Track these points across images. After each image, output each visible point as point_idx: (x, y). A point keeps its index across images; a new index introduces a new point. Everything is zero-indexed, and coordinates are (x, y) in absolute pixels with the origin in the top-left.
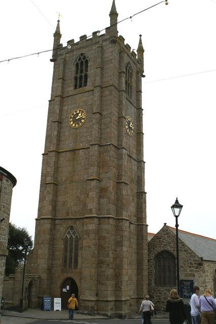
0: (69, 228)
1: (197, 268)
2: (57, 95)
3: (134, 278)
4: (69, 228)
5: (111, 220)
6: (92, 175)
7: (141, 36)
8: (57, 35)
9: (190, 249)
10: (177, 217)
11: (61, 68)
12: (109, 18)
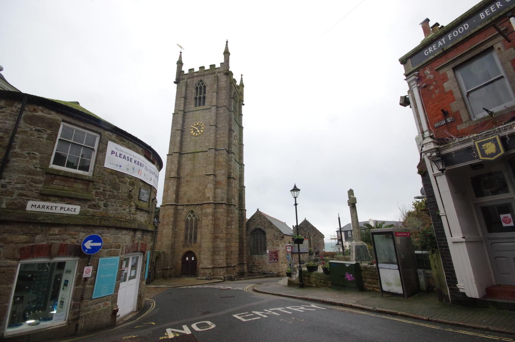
0: (190, 212)
1: (281, 240)
2: (181, 110)
4: (190, 212)
5: (224, 205)
6: (210, 171)
7: (242, 75)
8: (180, 63)
9: (276, 227)
10: (295, 198)
11: (184, 89)
12: (223, 56)
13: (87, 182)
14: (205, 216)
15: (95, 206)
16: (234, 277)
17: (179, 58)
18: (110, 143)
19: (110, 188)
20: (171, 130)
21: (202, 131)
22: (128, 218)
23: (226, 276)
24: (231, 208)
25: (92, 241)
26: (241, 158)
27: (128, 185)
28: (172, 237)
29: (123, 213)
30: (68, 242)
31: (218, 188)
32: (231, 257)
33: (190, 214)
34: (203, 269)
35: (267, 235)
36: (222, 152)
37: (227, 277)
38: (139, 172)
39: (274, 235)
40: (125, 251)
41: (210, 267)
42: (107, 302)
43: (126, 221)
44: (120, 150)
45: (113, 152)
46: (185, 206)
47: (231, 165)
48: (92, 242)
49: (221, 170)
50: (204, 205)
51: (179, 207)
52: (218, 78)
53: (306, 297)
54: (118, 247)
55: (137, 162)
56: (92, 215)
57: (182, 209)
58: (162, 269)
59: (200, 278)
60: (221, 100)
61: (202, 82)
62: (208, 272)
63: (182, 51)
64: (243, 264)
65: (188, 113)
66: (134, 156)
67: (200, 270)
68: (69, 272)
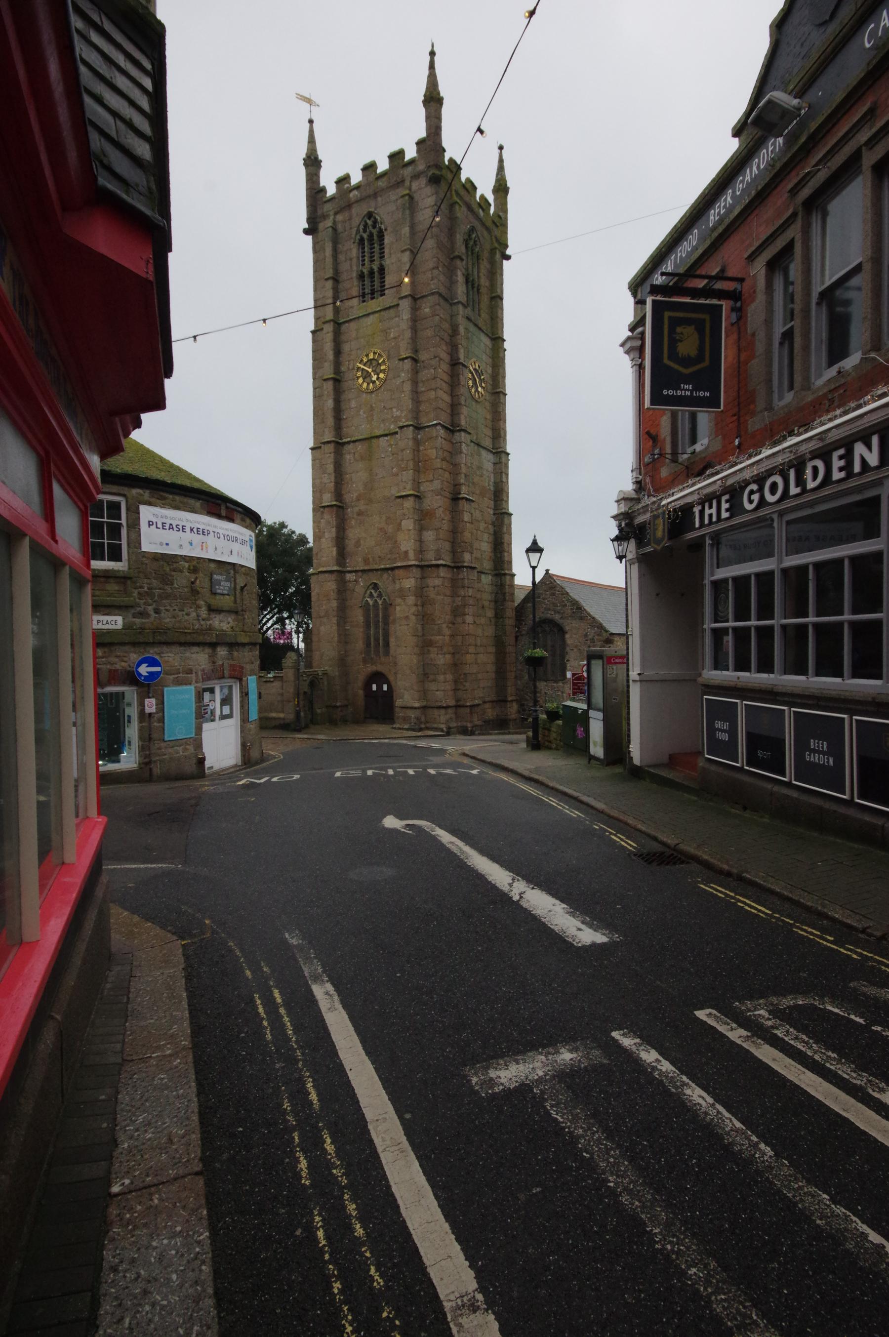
3: (491, 668)
5: (441, 568)
7: (501, 148)
8: (312, 163)
9: (589, 614)
10: (534, 568)
13: (122, 580)
14: (400, 597)
15: (143, 614)
16: (473, 727)
17: (309, 142)
18: (143, 509)
19: (159, 583)
20: (312, 380)
21: (382, 376)
22: (196, 627)
23: (453, 724)
24: (461, 576)
25: (147, 665)
26: (498, 433)
27: (187, 574)
28: (339, 642)
29: (186, 621)
30: (118, 667)
31: (427, 529)
32: (464, 686)
33: (371, 592)
34: (404, 710)
35: (567, 636)
36: (434, 432)
37: (457, 727)
38: (202, 546)
39: (586, 635)
40: (203, 678)
41: (417, 705)
42: (188, 747)
43: (194, 633)
44: (162, 517)
45: (150, 524)
46: (360, 574)
47: (460, 464)
48: (147, 666)
49: (432, 481)
50: (397, 571)
51: (349, 577)
52: (411, 198)
53: (498, 762)
54: (190, 672)
55: (195, 530)
56: (141, 628)
57: (355, 581)
58: (327, 707)
59: (397, 726)
60: (424, 273)
61: (372, 219)
62: (412, 714)
63: (314, 118)
64: (505, 701)
65: (347, 324)
66: (188, 521)
67: (397, 710)
68: (129, 705)
